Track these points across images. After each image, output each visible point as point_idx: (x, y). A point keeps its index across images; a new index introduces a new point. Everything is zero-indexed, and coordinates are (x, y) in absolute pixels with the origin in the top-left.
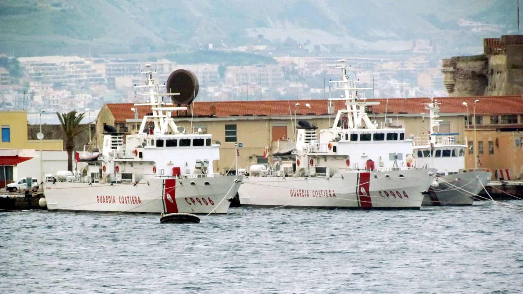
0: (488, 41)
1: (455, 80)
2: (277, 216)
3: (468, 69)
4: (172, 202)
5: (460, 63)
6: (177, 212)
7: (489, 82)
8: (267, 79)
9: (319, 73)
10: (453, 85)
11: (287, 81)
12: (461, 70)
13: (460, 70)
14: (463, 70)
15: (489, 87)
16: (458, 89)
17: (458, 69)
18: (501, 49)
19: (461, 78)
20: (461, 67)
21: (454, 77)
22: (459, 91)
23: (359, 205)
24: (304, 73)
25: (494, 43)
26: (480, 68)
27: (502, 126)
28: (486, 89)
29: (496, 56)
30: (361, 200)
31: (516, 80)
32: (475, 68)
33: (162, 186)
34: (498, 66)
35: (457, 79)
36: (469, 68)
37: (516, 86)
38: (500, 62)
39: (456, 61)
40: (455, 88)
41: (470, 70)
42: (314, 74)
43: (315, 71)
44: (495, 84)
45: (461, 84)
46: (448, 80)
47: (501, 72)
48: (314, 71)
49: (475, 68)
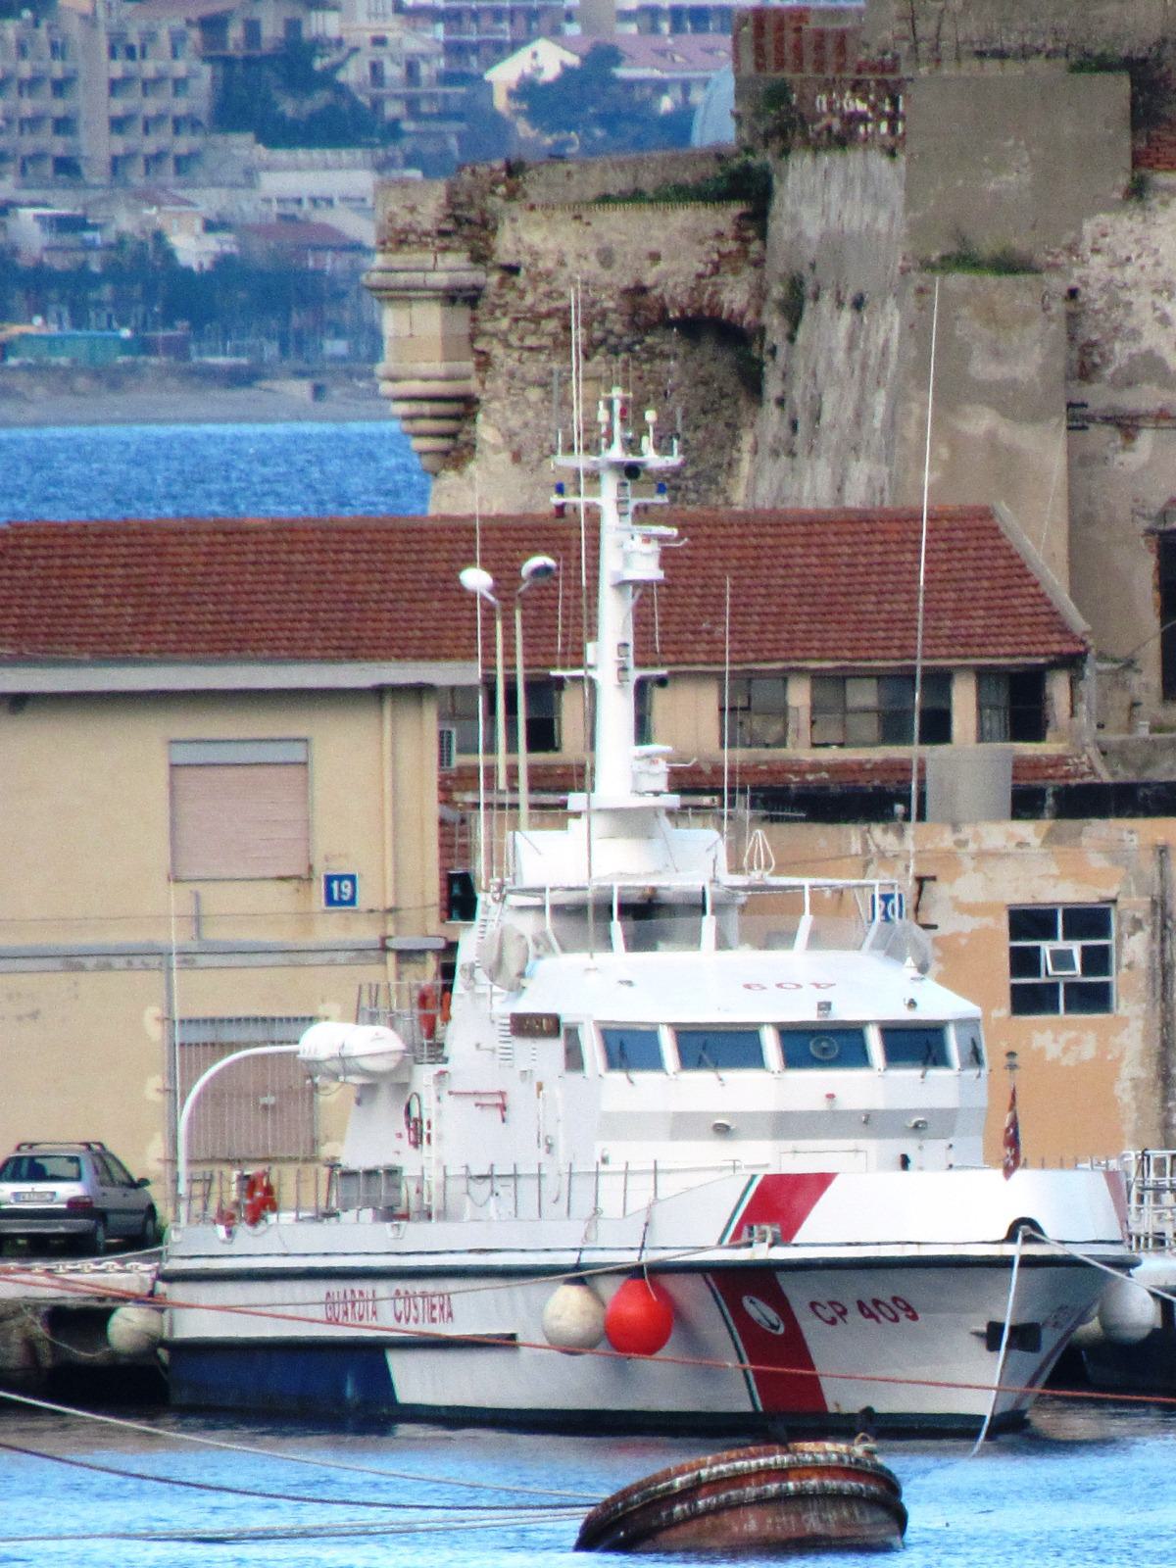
0: (769, 26)
1: (484, 361)
2: (258, 1490)
3: (592, 266)
4: (746, 1301)
5: (523, 217)
6: (984, 1417)
7: (772, 388)
8: (64, 125)
9: (550, 72)
10: (466, 407)
11: (243, 146)
12: (535, 279)
13: (521, 280)
14: (548, 275)
15: (771, 420)
16: (510, 435)
17: (512, 270)
18: (861, 107)
19: (530, 341)
20: (536, 255)
21: (472, 338)
22: (517, 457)
23: (754, 1404)
24: (393, 71)
25: (809, 54)
26: (693, 263)
27: (816, 767)
28: (747, 440)
29: (825, 159)
30: (752, 1362)
31: (982, 368)
32: (655, 257)
33: (496, 1088)
34: (836, 244)
35: (497, 351)
36: (606, 258)
37: (980, 422)
38: (855, 216)
39: (495, 203)
40: (486, 431)
41: (606, 276)
42: (504, 75)
43: (515, 46)
44: (817, 399)
45: (534, 394)
46: (424, 368)
47: (858, 304)
48: (502, 50)
49: (655, 257)
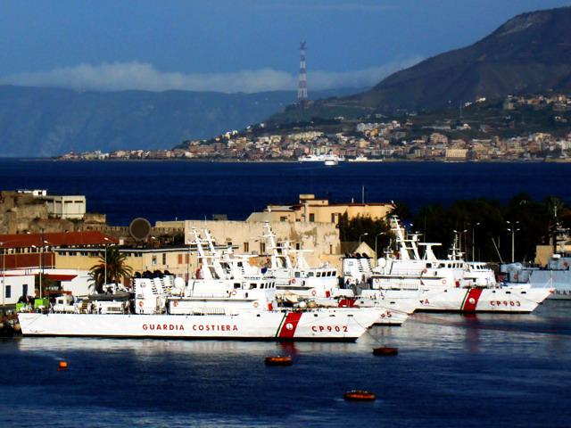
31: (72, 230)
